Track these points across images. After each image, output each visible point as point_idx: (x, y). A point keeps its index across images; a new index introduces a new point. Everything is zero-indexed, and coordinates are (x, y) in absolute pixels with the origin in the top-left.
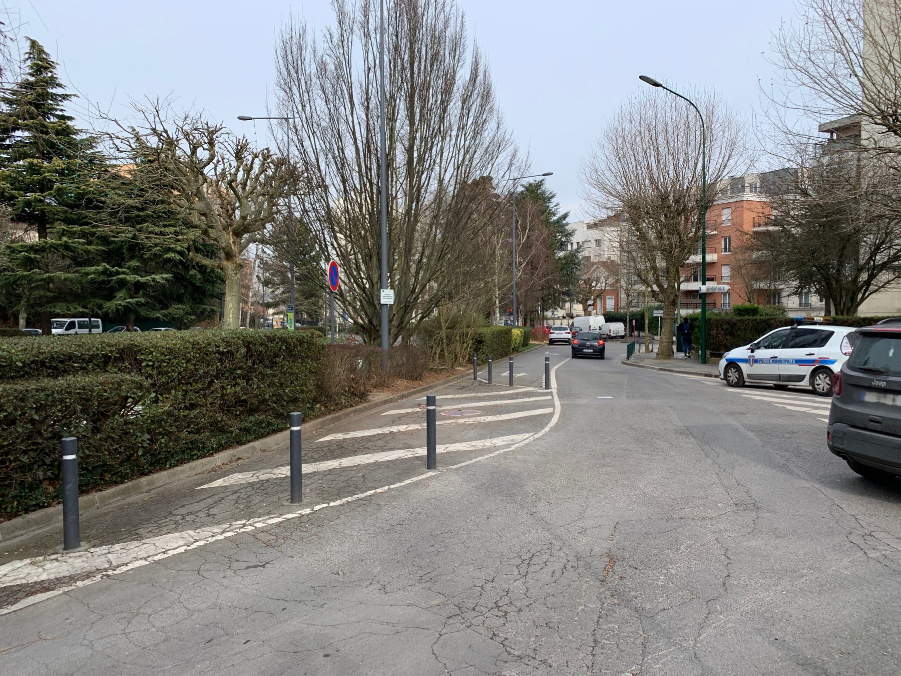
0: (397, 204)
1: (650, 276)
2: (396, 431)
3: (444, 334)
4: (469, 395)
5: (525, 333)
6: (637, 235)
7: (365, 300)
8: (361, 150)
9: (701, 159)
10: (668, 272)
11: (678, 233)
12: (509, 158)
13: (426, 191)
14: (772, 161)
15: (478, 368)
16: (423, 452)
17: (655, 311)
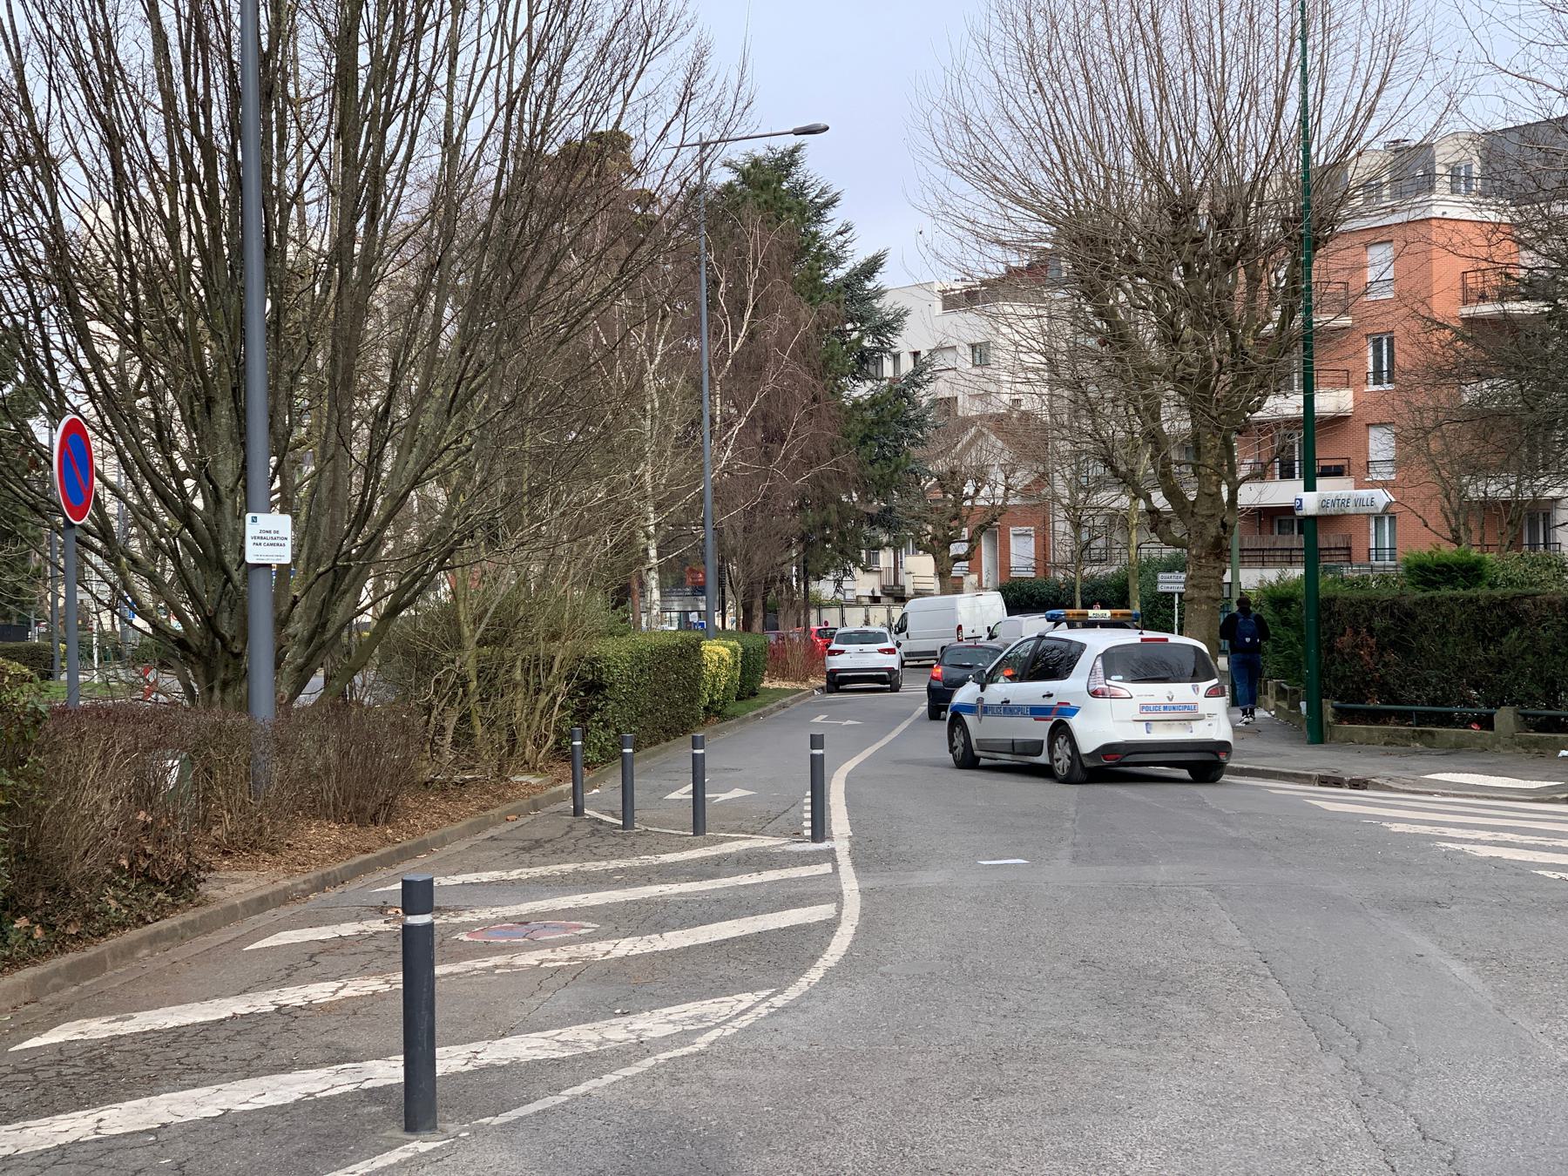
0: (302, 221)
1: (1145, 465)
2: (299, 1002)
3: (472, 662)
4: (555, 869)
5: (745, 654)
6: (1099, 331)
7: (192, 551)
8: (173, 38)
9: (1295, 87)
10: (1197, 449)
11: (1228, 325)
12: (682, 75)
13: (402, 179)
14: (1512, 95)
15: (589, 776)
16: (390, 1071)
17: (1160, 575)
